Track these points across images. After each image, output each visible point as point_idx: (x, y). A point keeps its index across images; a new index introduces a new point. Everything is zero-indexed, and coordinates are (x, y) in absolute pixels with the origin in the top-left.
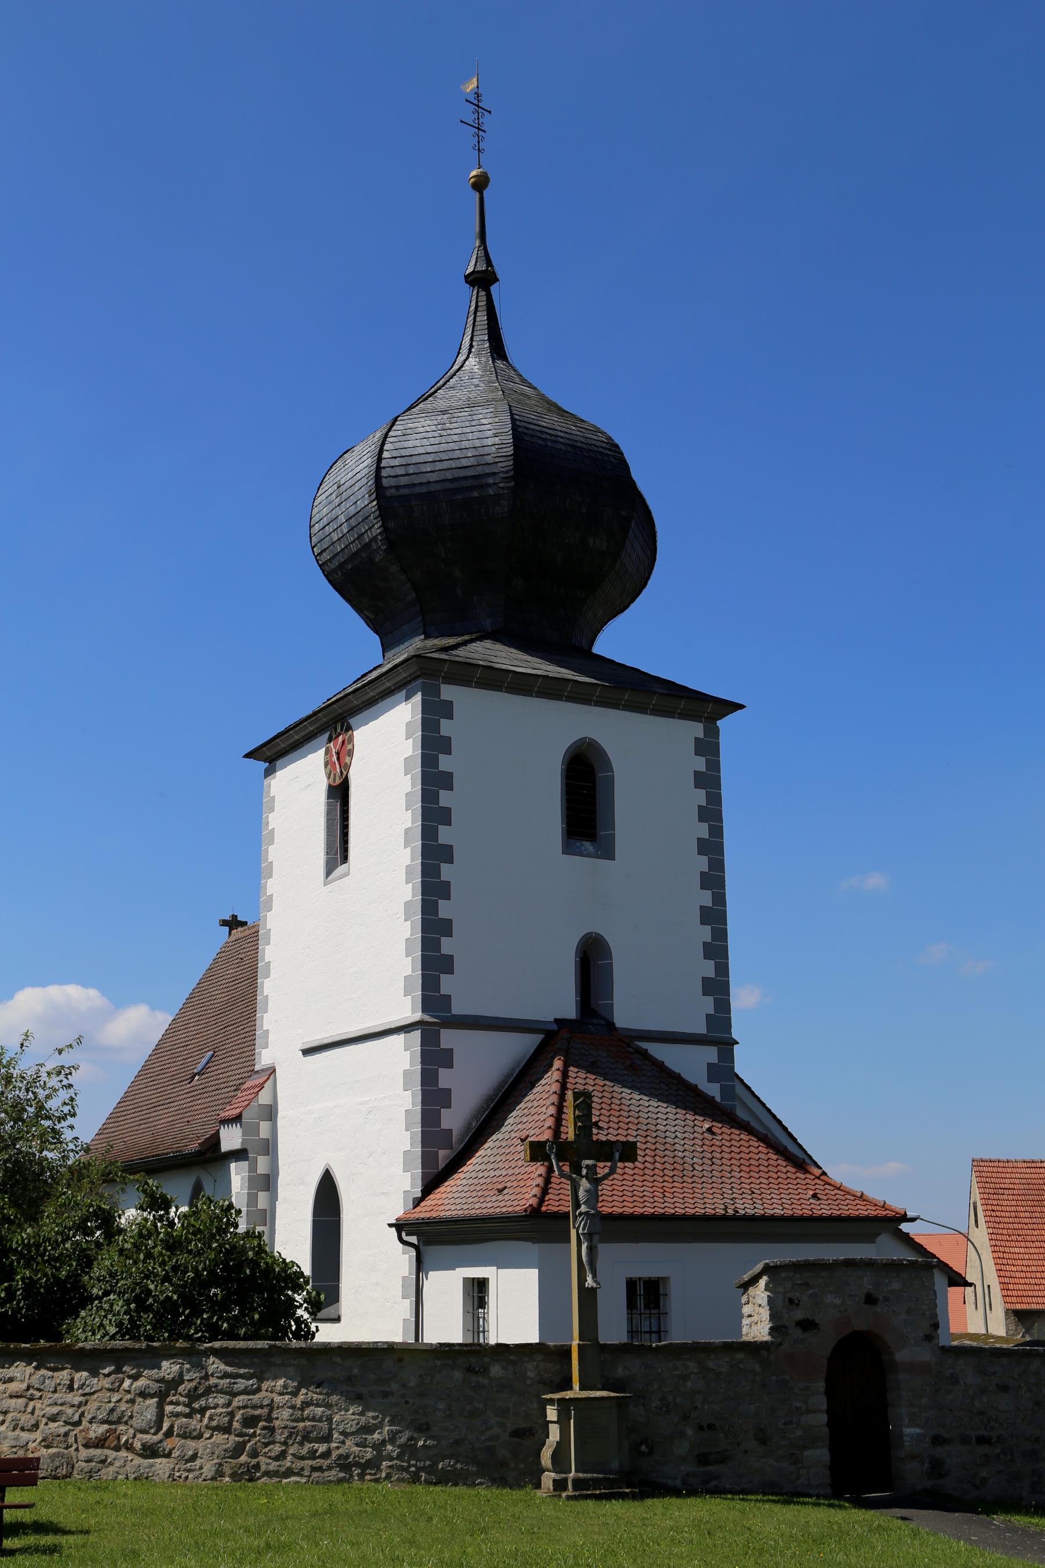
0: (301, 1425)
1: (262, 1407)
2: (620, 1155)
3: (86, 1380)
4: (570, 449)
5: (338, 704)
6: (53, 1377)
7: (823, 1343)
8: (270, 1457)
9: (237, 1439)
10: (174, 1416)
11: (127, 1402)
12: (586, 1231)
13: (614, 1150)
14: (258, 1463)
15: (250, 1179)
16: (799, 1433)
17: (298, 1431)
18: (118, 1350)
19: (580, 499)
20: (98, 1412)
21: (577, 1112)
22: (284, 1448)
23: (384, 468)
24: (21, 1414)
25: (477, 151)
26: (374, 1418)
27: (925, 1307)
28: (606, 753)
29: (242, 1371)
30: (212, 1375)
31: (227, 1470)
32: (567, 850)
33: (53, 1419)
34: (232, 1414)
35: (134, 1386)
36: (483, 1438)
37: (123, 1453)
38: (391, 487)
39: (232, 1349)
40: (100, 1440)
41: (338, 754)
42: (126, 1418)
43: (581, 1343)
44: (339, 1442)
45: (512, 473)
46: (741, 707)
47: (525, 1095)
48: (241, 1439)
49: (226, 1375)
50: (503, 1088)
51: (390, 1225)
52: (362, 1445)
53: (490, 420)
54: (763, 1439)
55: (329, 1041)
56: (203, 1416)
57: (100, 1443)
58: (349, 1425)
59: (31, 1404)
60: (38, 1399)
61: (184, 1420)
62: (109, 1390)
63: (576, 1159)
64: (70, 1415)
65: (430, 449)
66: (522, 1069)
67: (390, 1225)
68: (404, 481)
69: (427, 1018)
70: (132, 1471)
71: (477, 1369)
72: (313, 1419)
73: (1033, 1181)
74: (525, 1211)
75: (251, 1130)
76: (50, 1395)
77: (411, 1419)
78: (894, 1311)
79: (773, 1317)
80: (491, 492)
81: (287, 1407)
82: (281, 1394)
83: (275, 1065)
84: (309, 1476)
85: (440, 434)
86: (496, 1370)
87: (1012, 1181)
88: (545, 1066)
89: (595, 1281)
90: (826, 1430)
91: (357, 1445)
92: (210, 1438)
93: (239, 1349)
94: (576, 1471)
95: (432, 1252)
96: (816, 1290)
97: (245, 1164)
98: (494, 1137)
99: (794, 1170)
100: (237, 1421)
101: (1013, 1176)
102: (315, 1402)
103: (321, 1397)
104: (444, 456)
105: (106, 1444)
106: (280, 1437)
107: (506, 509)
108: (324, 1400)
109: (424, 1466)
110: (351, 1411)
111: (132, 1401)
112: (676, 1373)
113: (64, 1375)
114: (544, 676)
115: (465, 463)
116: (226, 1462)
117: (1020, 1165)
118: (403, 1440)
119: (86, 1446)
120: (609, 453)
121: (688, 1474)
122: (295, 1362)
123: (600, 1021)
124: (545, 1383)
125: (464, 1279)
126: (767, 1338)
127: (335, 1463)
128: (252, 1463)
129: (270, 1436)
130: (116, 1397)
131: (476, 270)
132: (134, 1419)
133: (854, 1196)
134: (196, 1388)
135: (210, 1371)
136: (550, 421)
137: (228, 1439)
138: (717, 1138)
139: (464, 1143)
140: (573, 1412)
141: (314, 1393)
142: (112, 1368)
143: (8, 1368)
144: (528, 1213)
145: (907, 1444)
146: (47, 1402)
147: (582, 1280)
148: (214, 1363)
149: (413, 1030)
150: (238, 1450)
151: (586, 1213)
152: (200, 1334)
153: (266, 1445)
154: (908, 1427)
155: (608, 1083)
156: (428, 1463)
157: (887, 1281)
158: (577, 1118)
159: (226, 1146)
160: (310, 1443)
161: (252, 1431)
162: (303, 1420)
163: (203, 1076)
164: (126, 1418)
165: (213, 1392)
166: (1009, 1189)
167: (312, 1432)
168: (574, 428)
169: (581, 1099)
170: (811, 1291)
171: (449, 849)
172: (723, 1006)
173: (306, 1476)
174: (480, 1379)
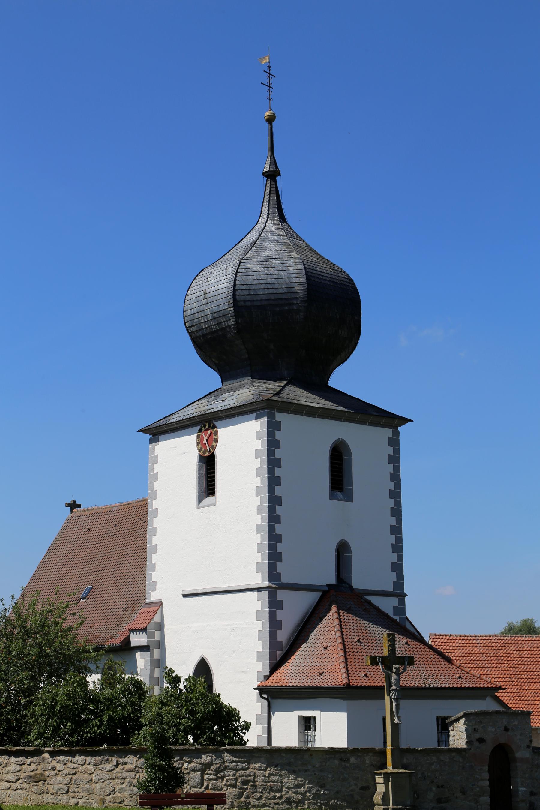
0: (269, 784)
1: (250, 776)
2: (408, 663)
4: (332, 284)
5: (209, 414)
7: (487, 749)
8: (255, 799)
9: (239, 790)
10: (209, 780)
12: (395, 698)
13: (405, 660)
14: (250, 801)
15: (151, 661)
16: (478, 789)
17: (267, 787)
18: (181, 750)
19: (337, 311)
21: (389, 643)
22: (261, 795)
23: (237, 290)
24: (133, 779)
25: (269, 100)
26: (301, 781)
27: (527, 733)
28: (349, 446)
29: (240, 760)
30: (227, 761)
31: (236, 804)
32: (332, 497)
34: (236, 779)
35: (189, 766)
36: (348, 790)
39: (236, 749)
41: (207, 440)
43: (393, 748)
44: (286, 792)
45: (306, 299)
46: (411, 421)
47: (318, 624)
48: (241, 791)
49: (233, 762)
50: (304, 620)
51: (255, 689)
52: (296, 793)
53: (293, 268)
54: (464, 793)
55: (204, 591)
56: (223, 780)
58: (290, 784)
59: (138, 775)
60: (141, 772)
61: (214, 782)
63: (389, 664)
65: (262, 282)
66: (313, 610)
67: (255, 689)
68: (248, 298)
69: (272, 585)
71: (345, 759)
72: (274, 782)
73: (466, 648)
74: (344, 685)
75: (151, 636)
77: (318, 782)
78: (515, 734)
79: (467, 737)
80: (295, 308)
81: (262, 776)
82: (259, 770)
83: (162, 601)
84: (273, 807)
85: (266, 273)
86: (353, 760)
87: (454, 648)
88: (326, 609)
89: (399, 720)
90: (489, 788)
91: (294, 793)
92: (227, 790)
94: (393, 805)
95: (276, 702)
96: (485, 725)
97: (148, 654)
98: (304, 645)
99: (447, 664)
100: (239, 783)
101: (454, 644)
102: (275, 774)
103: (277, 772)
104: (270, 287)
106: (259, 790)
107: (302, 317)
108: (279, 773)
109: (324, 803)
110: (291, 778)
112: (428, 762)
114: (323, 408)
115: (281, 291)
116: (235, 801)
117: (458, 638)
118: (314, 791)
120: (349, 284)
121: (433, 808)
122: (264, 756)
123: (346, 585)
124: (373, 766)
126: (465, 746)
127: (285, 801)
128: (247, 801)
129: (255, 789)
131: (270, 170)
133: (476, 677)
134: (219, 767)
135: (226, 759)
136: (321, 267)
137: (235, 790)
138: (411, 647)
139: (287, 648)
140: (391, 779)
141: (274, 770)
142: (178, 758)
143: (124, 758)
144: (345, 686)
145: (520, 795)
147: (392, 720)
148: (227, 756)
149: (263, 591)
150: (240, 795)
151: (396, 690)
152: (206, 743)
153: (253, 793)
154: (520, 787)
155: (358, 618)
156: (325, 801)
157: (512, 721)
158: (389, 646)
159: (134, 643)
160: (273, 792)
161: (246, 787)
162: (269, 782)
163: (89, 600)
165: (227, 769)
166: (452, 653)
167: (274, 787)
168: (331, 270)
169: (391, 637)
170: (483, 725)
171: (280, 498)
172: (400, 577)
173: (272, 807)
174: (346, 764)
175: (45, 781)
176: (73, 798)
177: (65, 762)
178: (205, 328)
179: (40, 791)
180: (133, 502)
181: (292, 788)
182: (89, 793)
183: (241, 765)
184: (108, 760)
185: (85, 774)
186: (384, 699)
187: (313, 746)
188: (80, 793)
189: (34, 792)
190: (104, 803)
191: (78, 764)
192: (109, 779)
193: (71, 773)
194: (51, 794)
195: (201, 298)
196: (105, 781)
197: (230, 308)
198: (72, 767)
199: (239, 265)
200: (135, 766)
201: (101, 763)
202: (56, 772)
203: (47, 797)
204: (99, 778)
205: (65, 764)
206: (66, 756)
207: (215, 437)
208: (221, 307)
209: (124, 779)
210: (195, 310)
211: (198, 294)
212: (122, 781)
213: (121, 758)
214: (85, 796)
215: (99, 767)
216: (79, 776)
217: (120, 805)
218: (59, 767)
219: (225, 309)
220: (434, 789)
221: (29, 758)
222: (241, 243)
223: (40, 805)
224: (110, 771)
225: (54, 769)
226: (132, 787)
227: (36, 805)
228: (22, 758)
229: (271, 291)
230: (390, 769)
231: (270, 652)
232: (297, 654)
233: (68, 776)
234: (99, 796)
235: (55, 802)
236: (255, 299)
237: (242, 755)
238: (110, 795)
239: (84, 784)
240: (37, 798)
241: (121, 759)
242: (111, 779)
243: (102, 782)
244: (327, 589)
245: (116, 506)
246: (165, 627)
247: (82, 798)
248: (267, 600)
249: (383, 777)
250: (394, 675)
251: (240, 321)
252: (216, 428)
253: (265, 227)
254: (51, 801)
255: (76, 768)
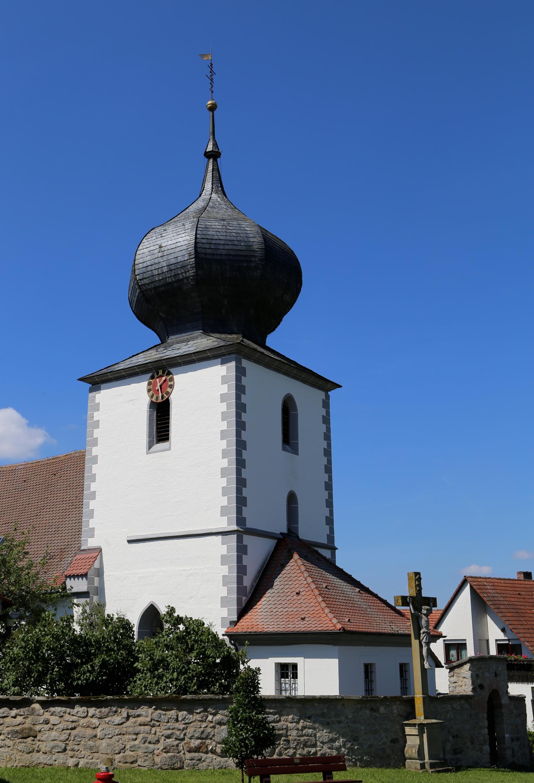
0: (302, 738)
1: (283, 729)
3: (186, 716)
4: (281, 250)
6: (166, 714)
11: (211, 727)
12: (427, 641)
20: (195, 733)
23: (198, 243)
24: (148, 734)
29: (271, 711)
33: (168, 737)
35: (214, 719)
36: (380, 744)
37: (210, 755)
38: (202, 253)
39: (267, 699)
40: (197, 748)
41: (161, 386)
42: (211, 736)
44: (321, 747)
45: (264, 257)
46: (340, 386)
54: (472, 742)
55: (156, 536)
57: (197, 750)
58: (325, 738)
59: (153, 729)
60: (157, 726)
62: (200, 721)
64: (179, 735)
65: (221, 238)
68: (209, 251)
70: (217, 764)
72: (308, 736)
75: (91, 582)
76: (165, 724)
79: (473, 683)
80: (253, 265)
82: (291, 723)
91: (329, 748)
93: (271, 699)
94: (429, 759)
98: (269, 591)
103: (311, 724)
105: (201, 750)
106: (293, 745)
107: (259, 274)
108: (312, 725)
109: (358, 759)
110: (325, 731)
111: (214, 727)
112: (444, 710)
113: (173, 713)
115: (240, 248)
119: (189, 751)
124: (401, 716)
125: (275, 663)
130: (204, 725)
132: (215, 737)
140: (426, 730)
141: (307, 722)
142: (202, 709)
143: (136, 709)
146: (163, 728)
147: (422, 666)
153: (286, 749)
156: (360, 757)
160: (307, 748)
162: (303, 736)
164: (211, 736)
167: (308, 742)
172: (332, 530)
174: (376, 714)
175: (35, 737)
176: (71, 757)
177: (62, 714)
178: (158, 280)
179: (29, 750)
180: (42, 460)
181: (326, 743)
182: (92, 752)
183: (272, 717)
184: (116, 712)
185: (88, 728)
186: (409, 645)
187: (293, 695)
188: (81, 751)
189: (21, 750)
190: (112, 763)
191: (79, 717)
192: (117, 735)
193: (70, 727)
194: (43, 753)
195: (156, 251)
196: (112, 737)
197: (191, 259)
198: (71, 720)
199: (198, 222)
200: (150, 718)
201: (107, 715)
202: (49, 726)
203: (37, 756)
204: (106, 733)
205: (62, 717)
206: (63, 707)
207: (170, 383)
208: (180, 259)
209: (137, 734)
210: (149, 263)
211: (152, 248)
212: (134, 737)
213: (133, 709)
214: (88, 755)
215: (105, 719)
216: (79, 731)
217: (133, 765)
218: (54, 720)
219: (184, 261)
220: (451, 739)
221: (14, 709)
222: (187, 210)
223: (28, 767)
224: (119, 725)
225: (47, 722)
226: (147, 744)
227: (23, 766)
228: (5, 709)
229: (230, 247)
230: (420, 718)
231: (237, 597)
232: (263, 599)
233: (65, 731)
234: (106, 755)
235: (49, 762)
236: (215, 253)
237: (273, 705)
238: (119, 753)
239: (86, 740)
240: (24, 757)
241: (132, 711)
242: (120, 734)
243: (109, 738)
244: (281, 537)
245: (22, 465)
246: (105, 574)
247: (83, 758)
248: (235, 544)
249: (417, 727)
250: (423, 616)
251: (200, 272)
252: (172, 374)
253: (211, 197)
254: (43, 761)
255: (75, 722)
